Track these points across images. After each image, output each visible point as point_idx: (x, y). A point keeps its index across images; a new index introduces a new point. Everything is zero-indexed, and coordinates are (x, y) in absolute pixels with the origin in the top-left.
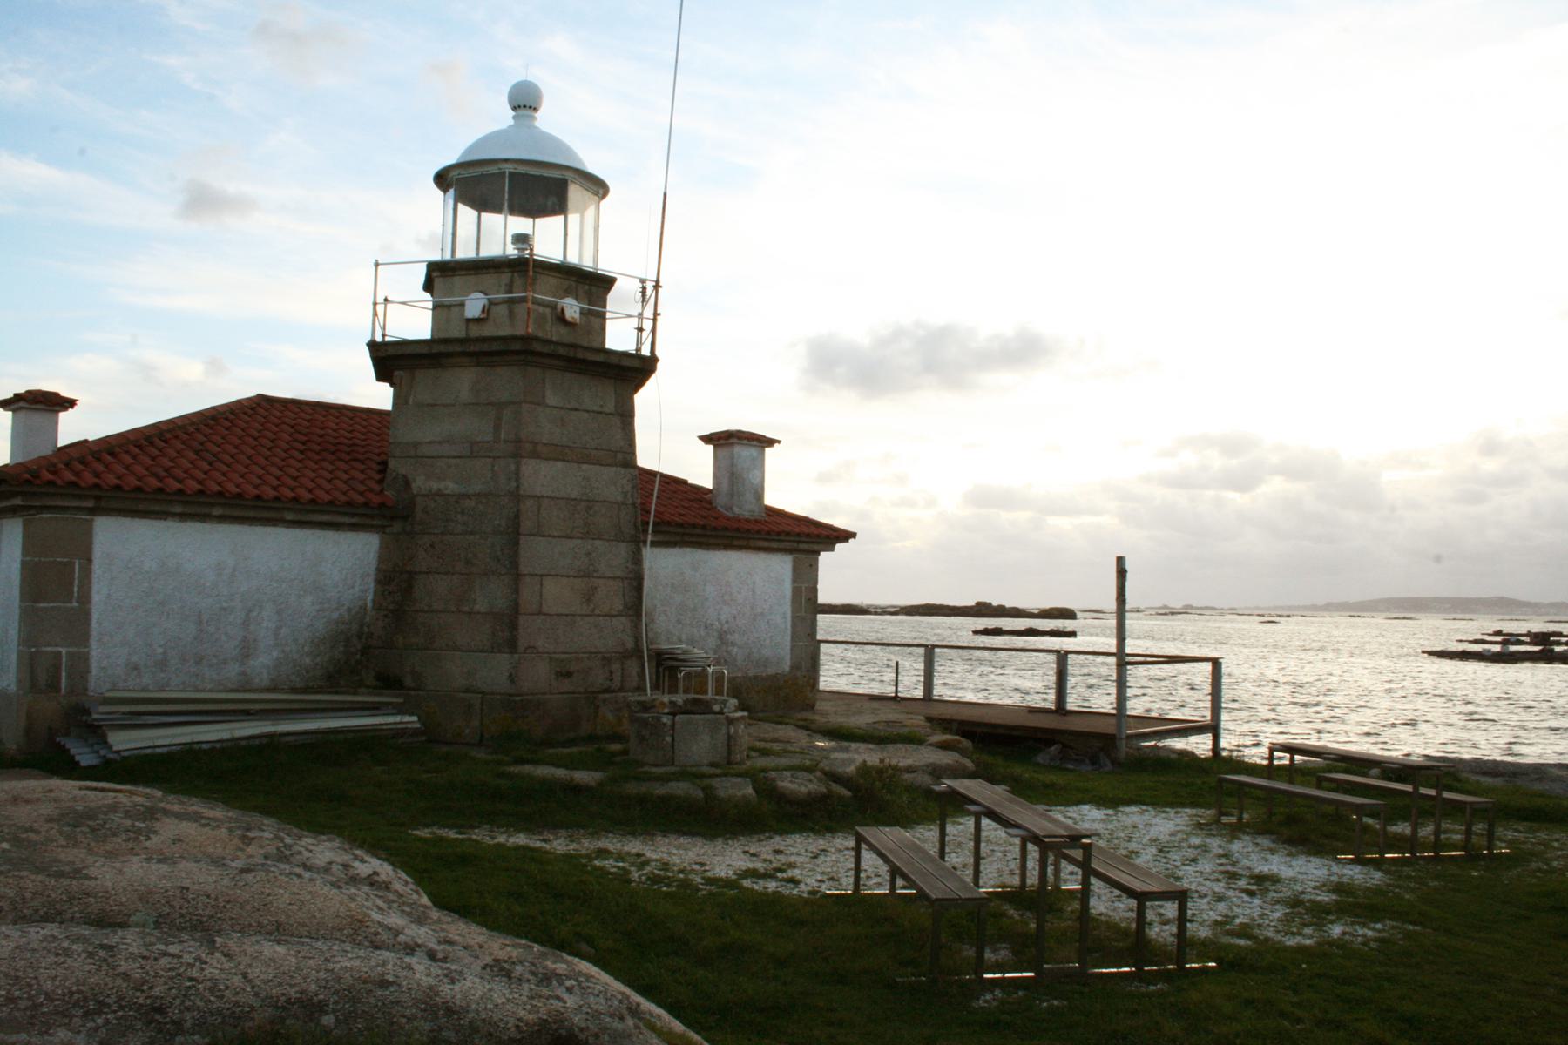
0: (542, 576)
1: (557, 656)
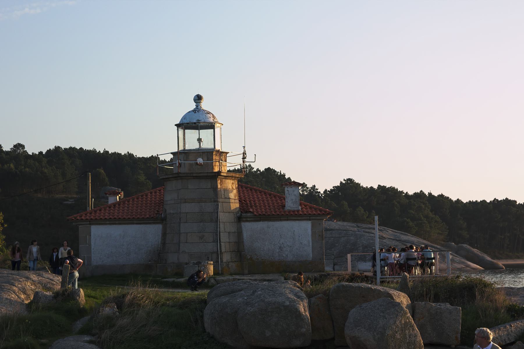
0: (187, 233)
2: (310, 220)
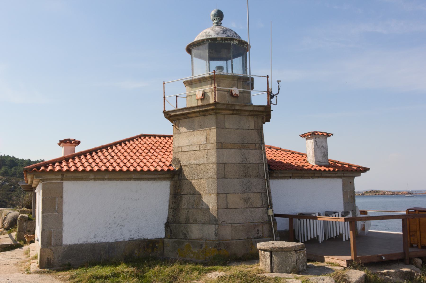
0: (227, 193)
1: (235, 225)
2: (341, 177)
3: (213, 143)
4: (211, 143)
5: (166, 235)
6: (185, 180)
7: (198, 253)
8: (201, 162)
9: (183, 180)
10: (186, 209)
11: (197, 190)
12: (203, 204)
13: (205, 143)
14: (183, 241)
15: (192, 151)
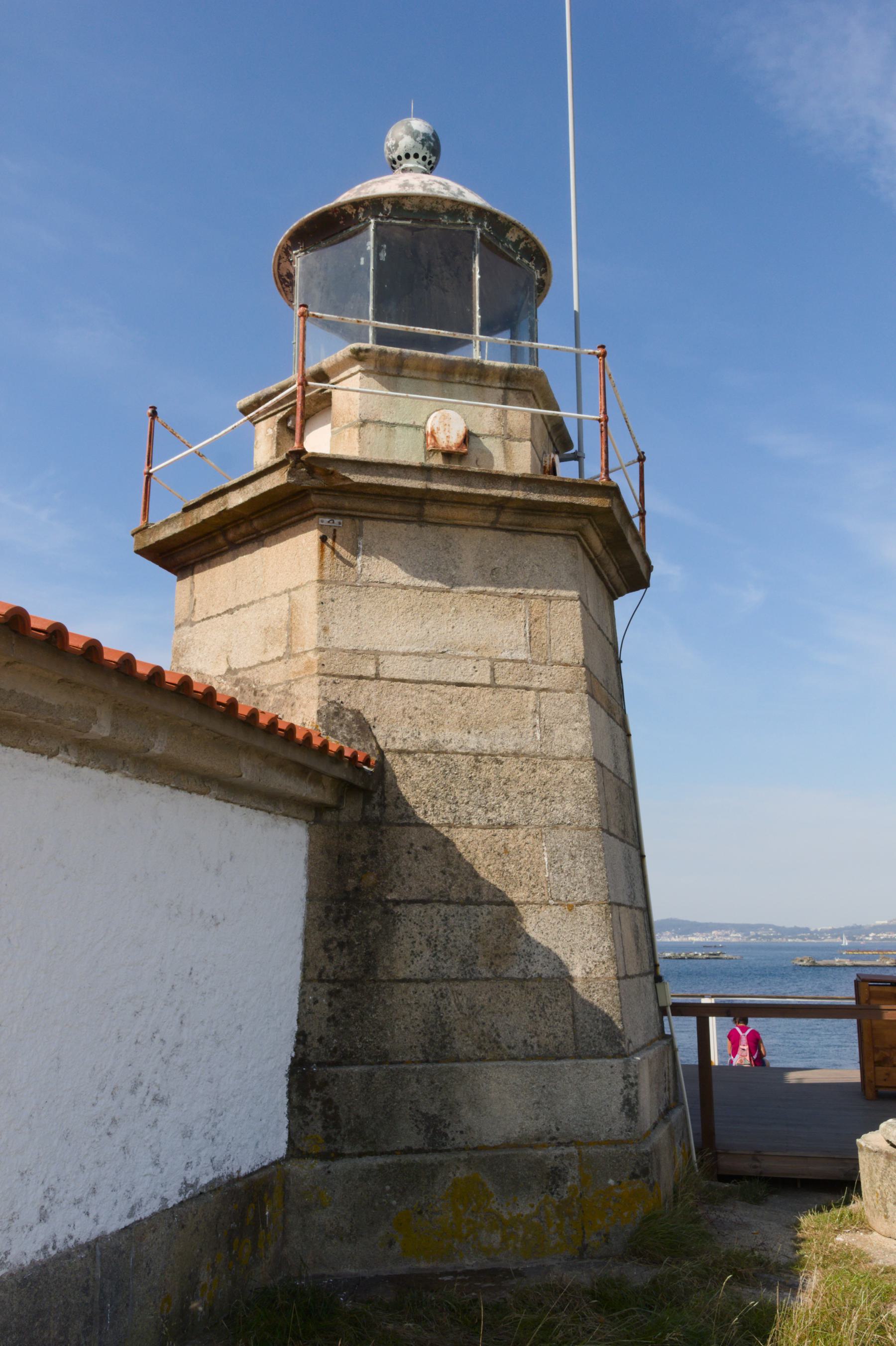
3: (566, 665)
4: (554, 663)
5: (290, 1142)
6: (409, 825)
7: (535, 1220)
8: (502, 743)
9: (399, 825)
10: (427, 982)
11: (492, 881)
12: (529, 955)
13: (522, 655)
14: (432, 1164)
15: (448, 684)
